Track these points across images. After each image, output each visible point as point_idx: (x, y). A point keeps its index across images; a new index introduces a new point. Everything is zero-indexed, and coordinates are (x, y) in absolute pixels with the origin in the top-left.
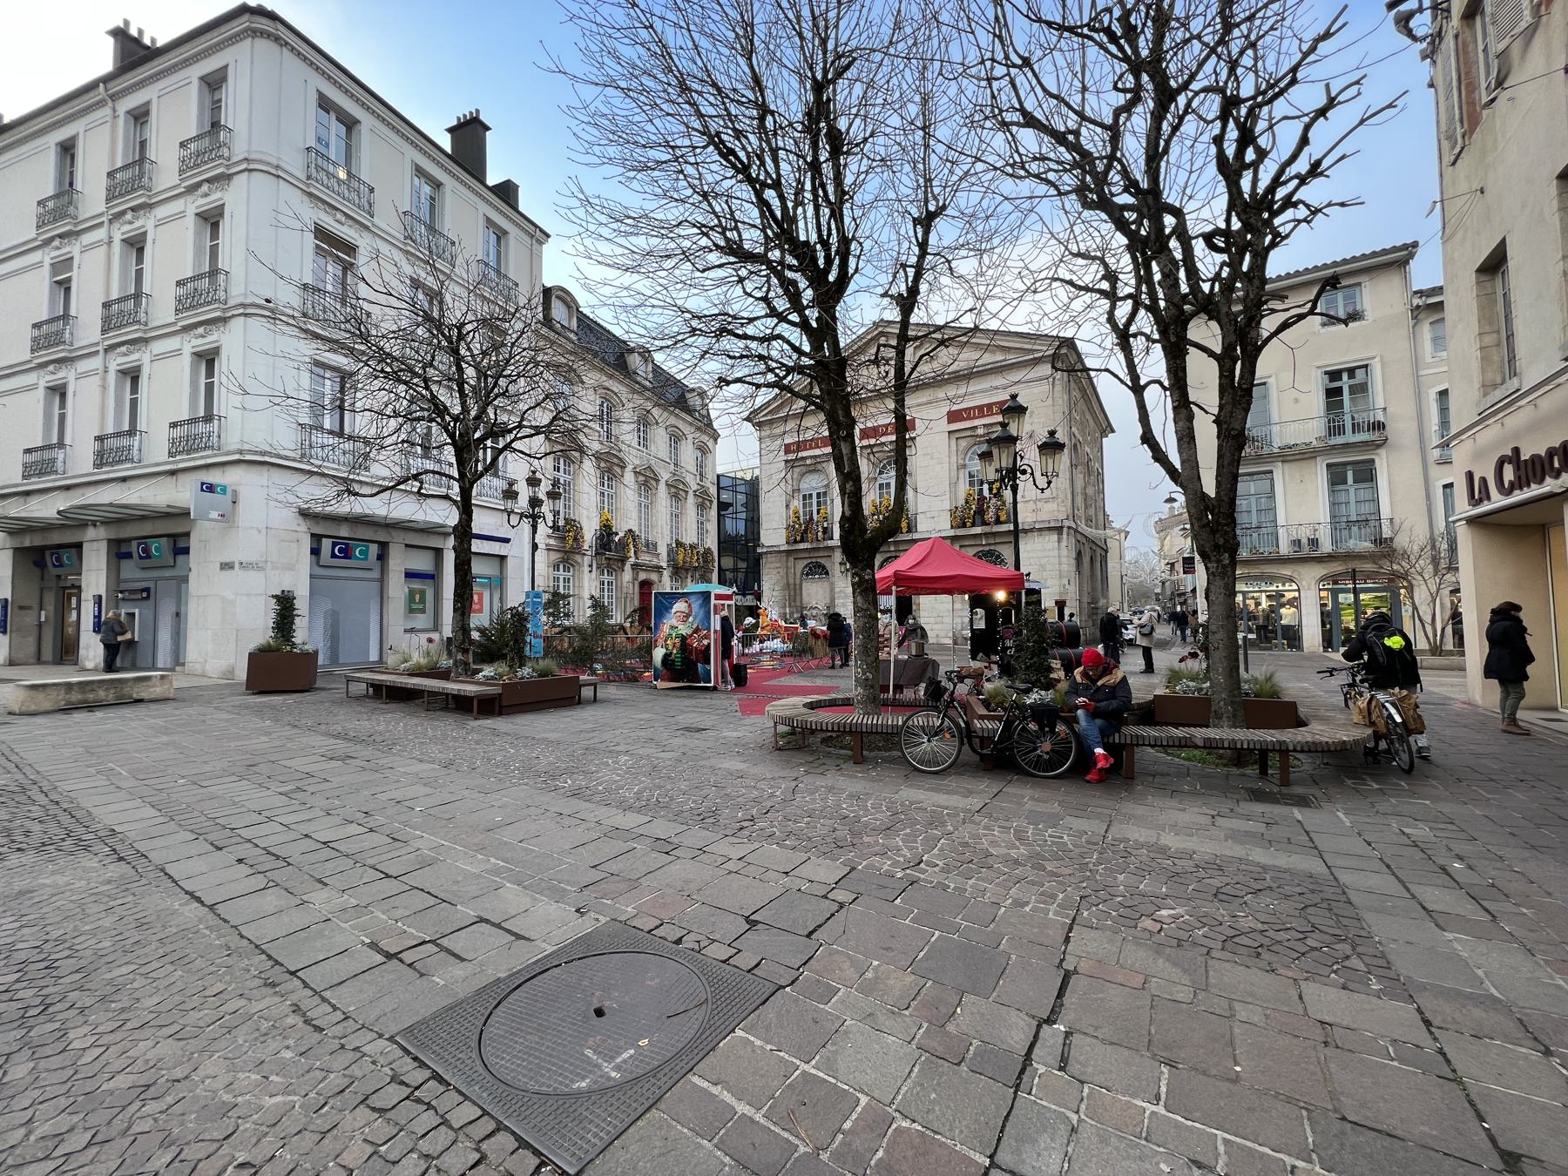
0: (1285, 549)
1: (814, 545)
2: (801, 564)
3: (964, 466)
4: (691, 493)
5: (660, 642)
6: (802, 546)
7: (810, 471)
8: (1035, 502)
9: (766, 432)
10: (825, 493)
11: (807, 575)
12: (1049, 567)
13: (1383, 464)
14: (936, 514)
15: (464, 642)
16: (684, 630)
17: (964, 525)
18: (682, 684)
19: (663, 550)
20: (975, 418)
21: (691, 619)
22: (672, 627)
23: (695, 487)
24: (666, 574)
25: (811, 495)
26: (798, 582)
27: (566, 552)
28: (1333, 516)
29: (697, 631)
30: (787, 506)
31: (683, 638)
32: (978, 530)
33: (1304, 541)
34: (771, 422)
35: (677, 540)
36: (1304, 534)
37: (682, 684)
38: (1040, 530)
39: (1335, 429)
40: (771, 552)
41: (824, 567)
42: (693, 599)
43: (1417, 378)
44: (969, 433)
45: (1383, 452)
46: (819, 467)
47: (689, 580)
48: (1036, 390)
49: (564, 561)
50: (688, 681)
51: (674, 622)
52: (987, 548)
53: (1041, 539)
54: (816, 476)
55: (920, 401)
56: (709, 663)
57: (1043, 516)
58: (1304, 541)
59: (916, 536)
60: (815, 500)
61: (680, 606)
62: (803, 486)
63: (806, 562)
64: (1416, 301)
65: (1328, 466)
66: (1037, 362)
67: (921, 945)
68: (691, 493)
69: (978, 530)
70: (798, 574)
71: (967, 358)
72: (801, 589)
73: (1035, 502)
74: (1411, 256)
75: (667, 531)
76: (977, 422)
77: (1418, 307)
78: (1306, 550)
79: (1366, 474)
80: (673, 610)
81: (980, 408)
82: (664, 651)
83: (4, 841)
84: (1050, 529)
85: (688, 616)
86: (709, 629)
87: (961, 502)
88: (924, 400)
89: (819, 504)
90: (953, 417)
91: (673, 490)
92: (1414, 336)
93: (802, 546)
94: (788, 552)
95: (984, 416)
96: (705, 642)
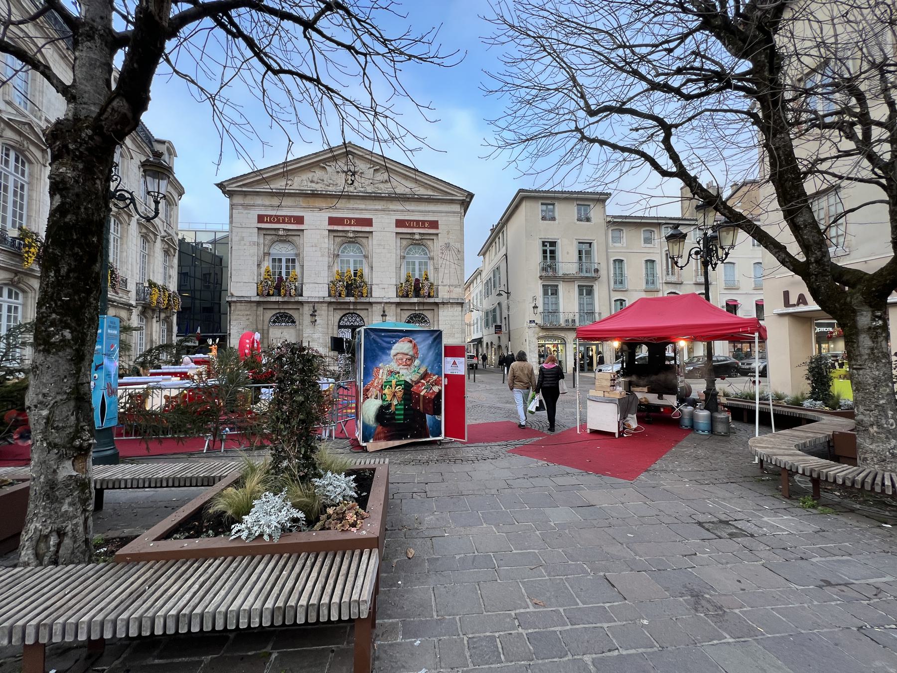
0: (563, 323)
1: (286, 299)
2: (269, 314)
3: (404, 257)
4: (159, 238)
5: (374, 391)
6: (273, 299)
7: (281, 241)
8: (449, 286)
9: (238, 200)
10: (293, 261)
11: (274, 322)
12: (456, 326)
13: (596, 288)
14: (386, 286)
15: (78, 431)
16: (408, 375)
17: (407, 296)
18: (397, 443)
19: (132, 287)
20: (413, 227)
21: (417, 362)
22: (391, 373)
23: (163, 234)
24: (135, 312)
25: (280, 260)
26: (266, 328)
27: (16, 273)
28: (580, 310)
29: (425, 376)
30: (259, 265)
31: (407, 386)
32: (415, 300)
33: (570, 320)
34: (245, 194)
35: (149, 281)
36: (571, 317)
37: (397, 443)
38: (452, 303)
39: (581, 270)
40: (241, 302)
41: (291, 317)
42: (418, 338)
43: (607, 252)
44: (409, 236)
45: (597, 282)
46: (290, 238)
47: (154, 320)
48: (451, 219)
49: (12, 284)
50: (412, 437)
51: (394, 366)
52: (417, 312)
53: (452, 309)
54: (286, 245)
55: (377, 207)
56: (439, 413)
57: (454, 295)
58: (570, 320)
59: (372, 300)
60: (284, 264)
61: (402, 347)
62: (272, 251)
63: (274, 312)
64: (609, 219)
65: (579, 286)
66: (452, 202)
67: (654, 637)
68: (159, 238)
69: (415, 300)
70: (266, 322)
71: (402, 187)
72: (268, 333)
73: (449, 286)
74: (609, 198)
75: (136, 269)
76: (415, 231)
77: (609, 222)
78: (570, 326)
79: (590, 292)
80: (393, 352)
81: (418, 222)
82: (379, 402)
83: (872, 2)
84: (457, 303)
85: (412, 359)
86: (439, 373)
87: (403, 281)
88: (380, 207)
89: (287, 267)
90: (400, 223)
91: (144, 230)
92: (606, 235)
93: (273, 299)
94: (258, 303)
95: (419, 227)
96: (436, 389)
